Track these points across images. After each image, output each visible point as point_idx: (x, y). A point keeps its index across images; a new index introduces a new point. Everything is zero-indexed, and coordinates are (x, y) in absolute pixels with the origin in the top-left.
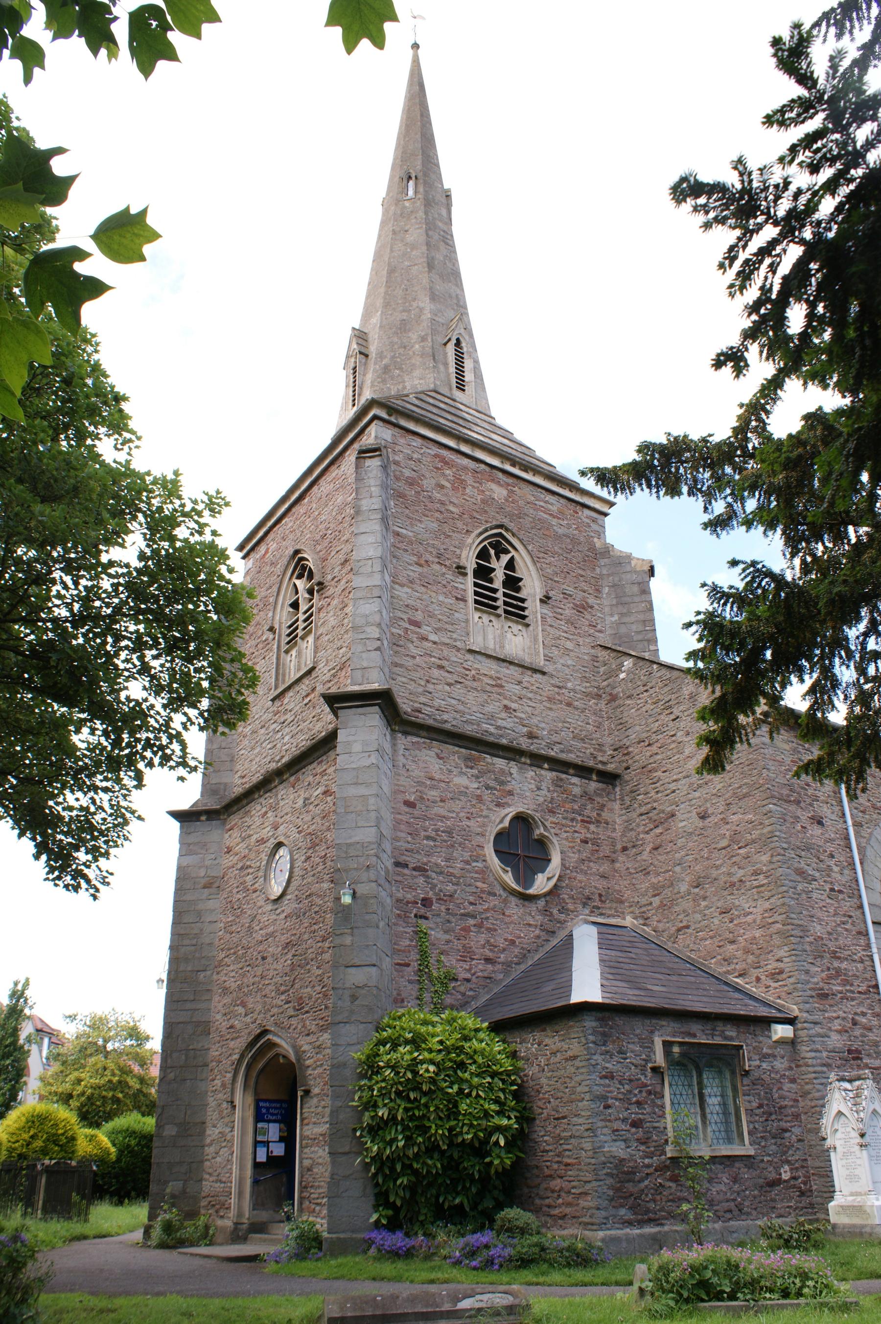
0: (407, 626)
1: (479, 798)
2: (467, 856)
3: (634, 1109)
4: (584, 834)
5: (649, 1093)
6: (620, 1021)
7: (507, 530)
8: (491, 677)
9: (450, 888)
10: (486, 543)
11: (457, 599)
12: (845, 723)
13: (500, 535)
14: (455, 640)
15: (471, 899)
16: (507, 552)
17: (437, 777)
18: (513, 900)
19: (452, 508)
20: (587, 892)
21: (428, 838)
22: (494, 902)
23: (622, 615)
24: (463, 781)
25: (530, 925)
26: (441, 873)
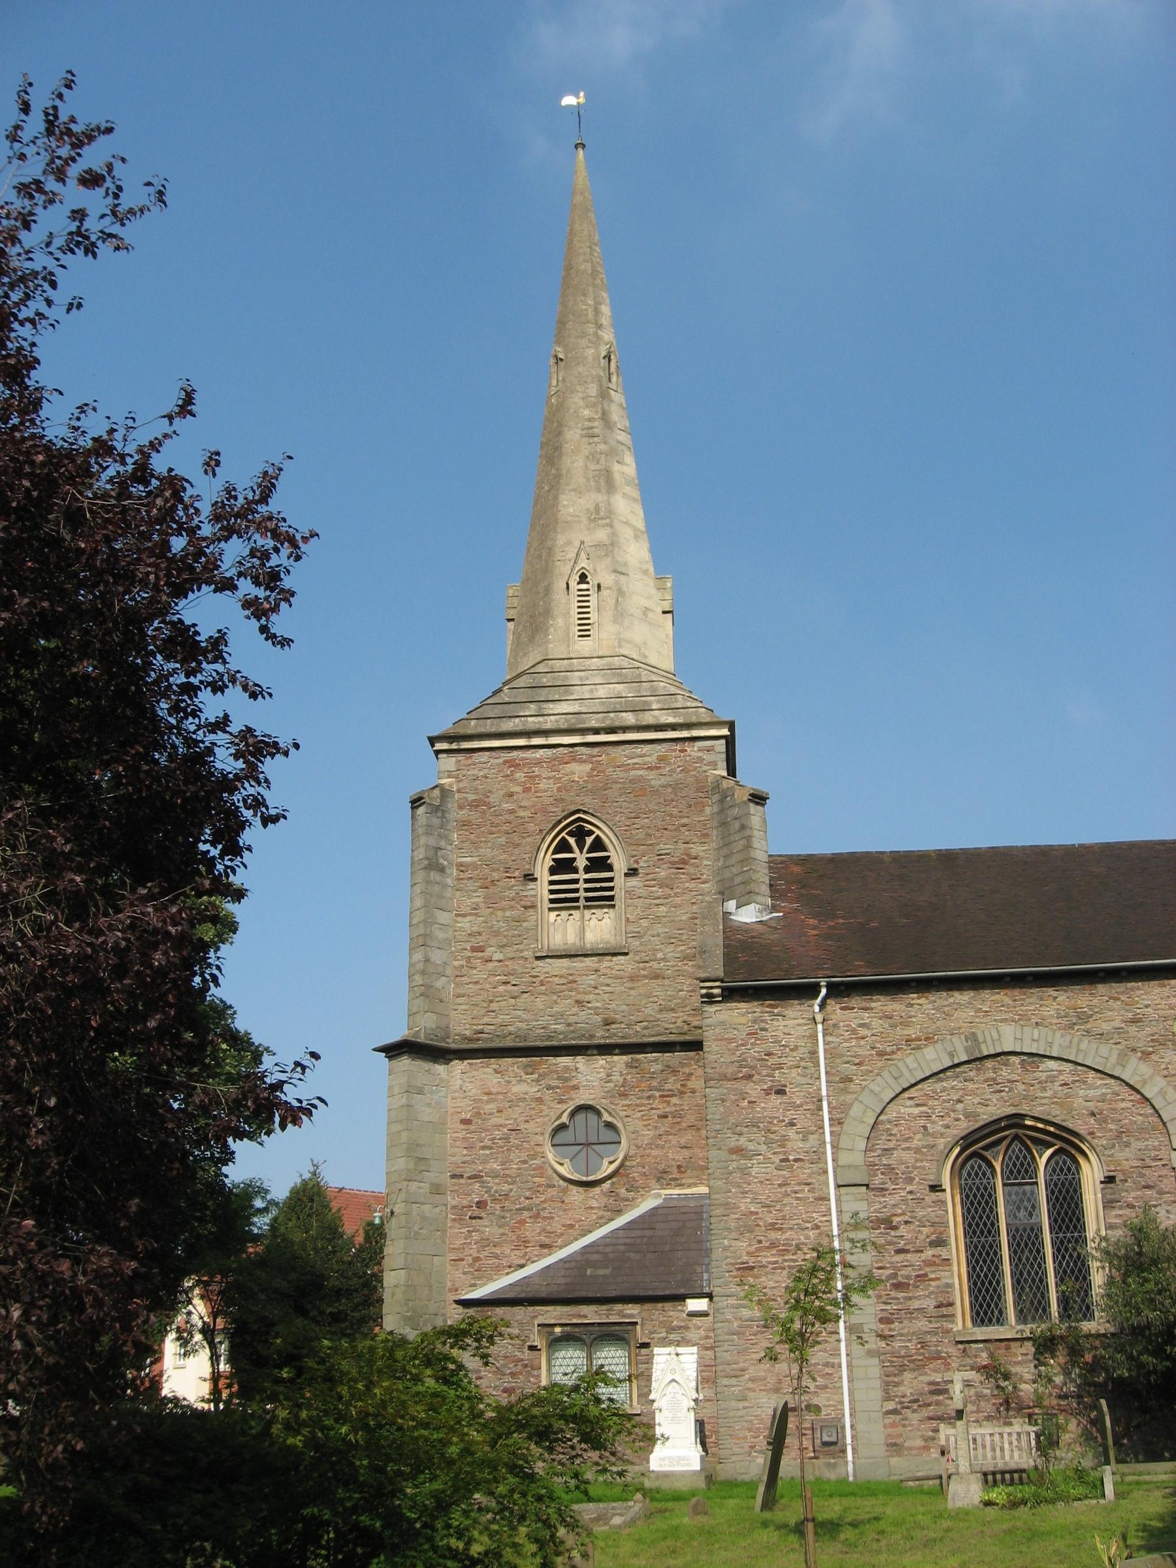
0: (470, 954)
1: (540, 1100)
2: (524, 1156)
3: (507, 1378)
4: (663, 1108)
5: (526, 1366)
6: (564, 1295)
7: (585, 812)
8: (562, 977)
9: (506, 1187)
10: (563, 834)
11: (525, 908)
12: (235, 1174)
13: (579, 819)
14: (522, 951)
15: (528, 1194)
16: (591, 833)
17: (494, 1090)
18: (574, 1189)
19: (522, 813)
20: (661, 1167)
21: (483, 1148)
22: (552, 1192)
23: (726, 857)
24: (523, 1088)
25: (591, 1208)
26: (497, 1177)
